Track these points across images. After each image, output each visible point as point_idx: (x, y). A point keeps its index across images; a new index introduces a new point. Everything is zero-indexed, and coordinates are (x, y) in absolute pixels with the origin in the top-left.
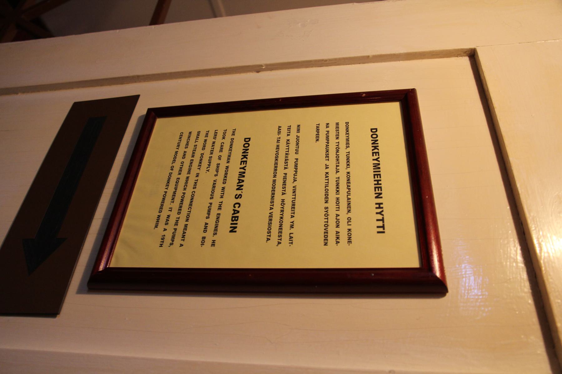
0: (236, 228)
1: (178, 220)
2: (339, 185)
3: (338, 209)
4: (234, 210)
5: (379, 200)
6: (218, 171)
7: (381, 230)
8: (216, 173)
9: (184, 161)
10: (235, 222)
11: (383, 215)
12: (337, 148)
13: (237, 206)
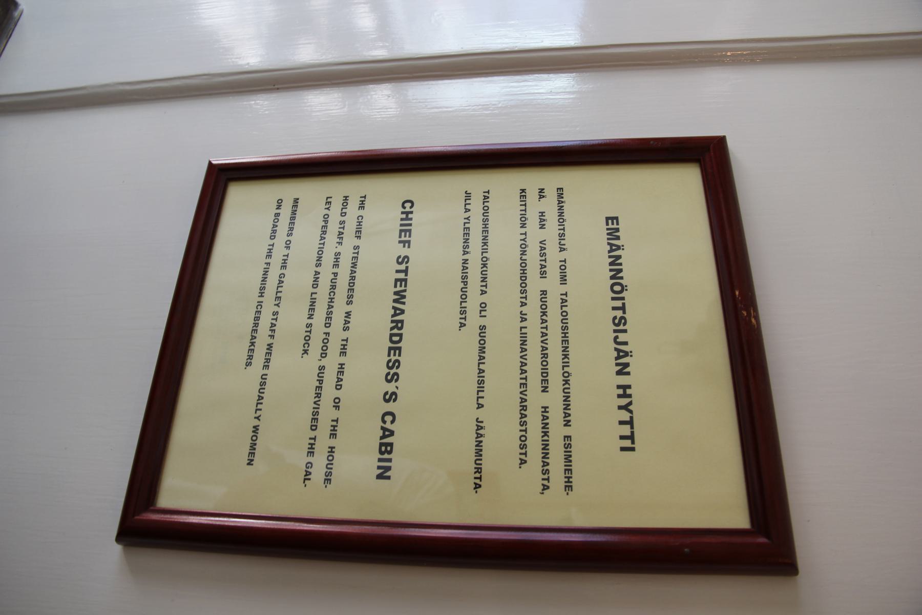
0: (388, 469)
2: (568, 351)
4: (382, 428)
5: (623, 380)
7: (627, 443)
11: (631, 412)
12: (523, 246)
13: (388, 418)
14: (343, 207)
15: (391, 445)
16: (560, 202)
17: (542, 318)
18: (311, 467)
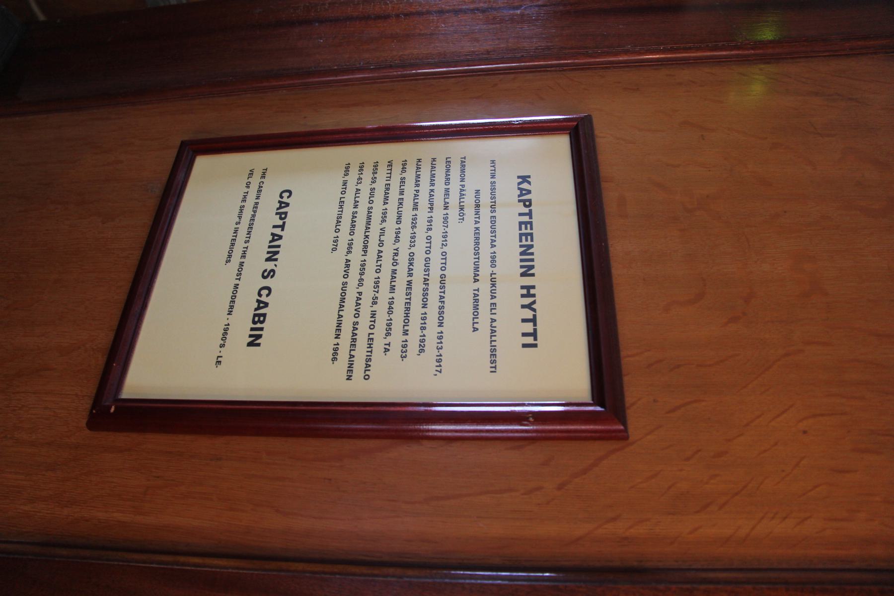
1: (246, 251)
3: (493, 369)
5: (527, 281)
6: (241, 217)
7: (530, 340)
8: (237, 220)
9: (251, 182)
10: (259, 325)
11: (534, 310)
14: (405, 324)
16: (386, 193)
17: (520, 186)
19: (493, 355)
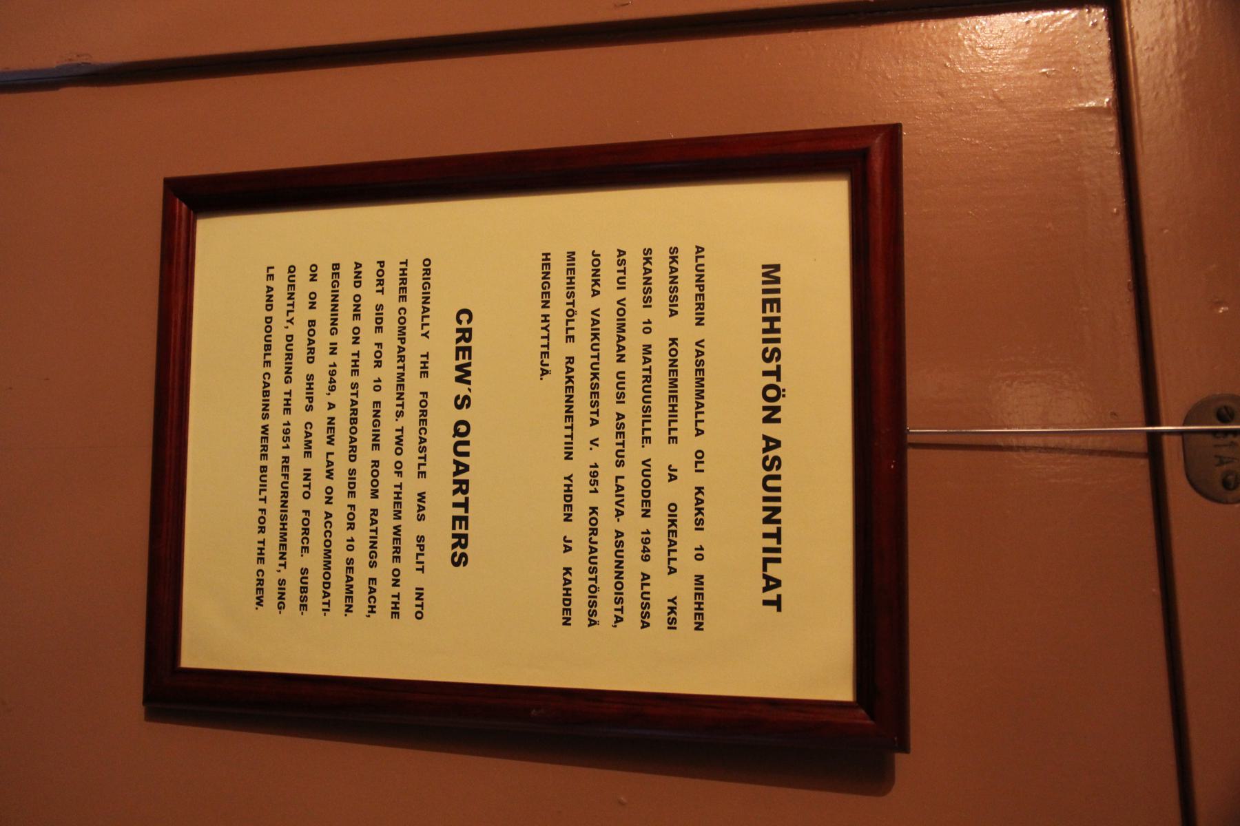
15: (269, 391)
18: (379, 425)
19: (595, 393)
